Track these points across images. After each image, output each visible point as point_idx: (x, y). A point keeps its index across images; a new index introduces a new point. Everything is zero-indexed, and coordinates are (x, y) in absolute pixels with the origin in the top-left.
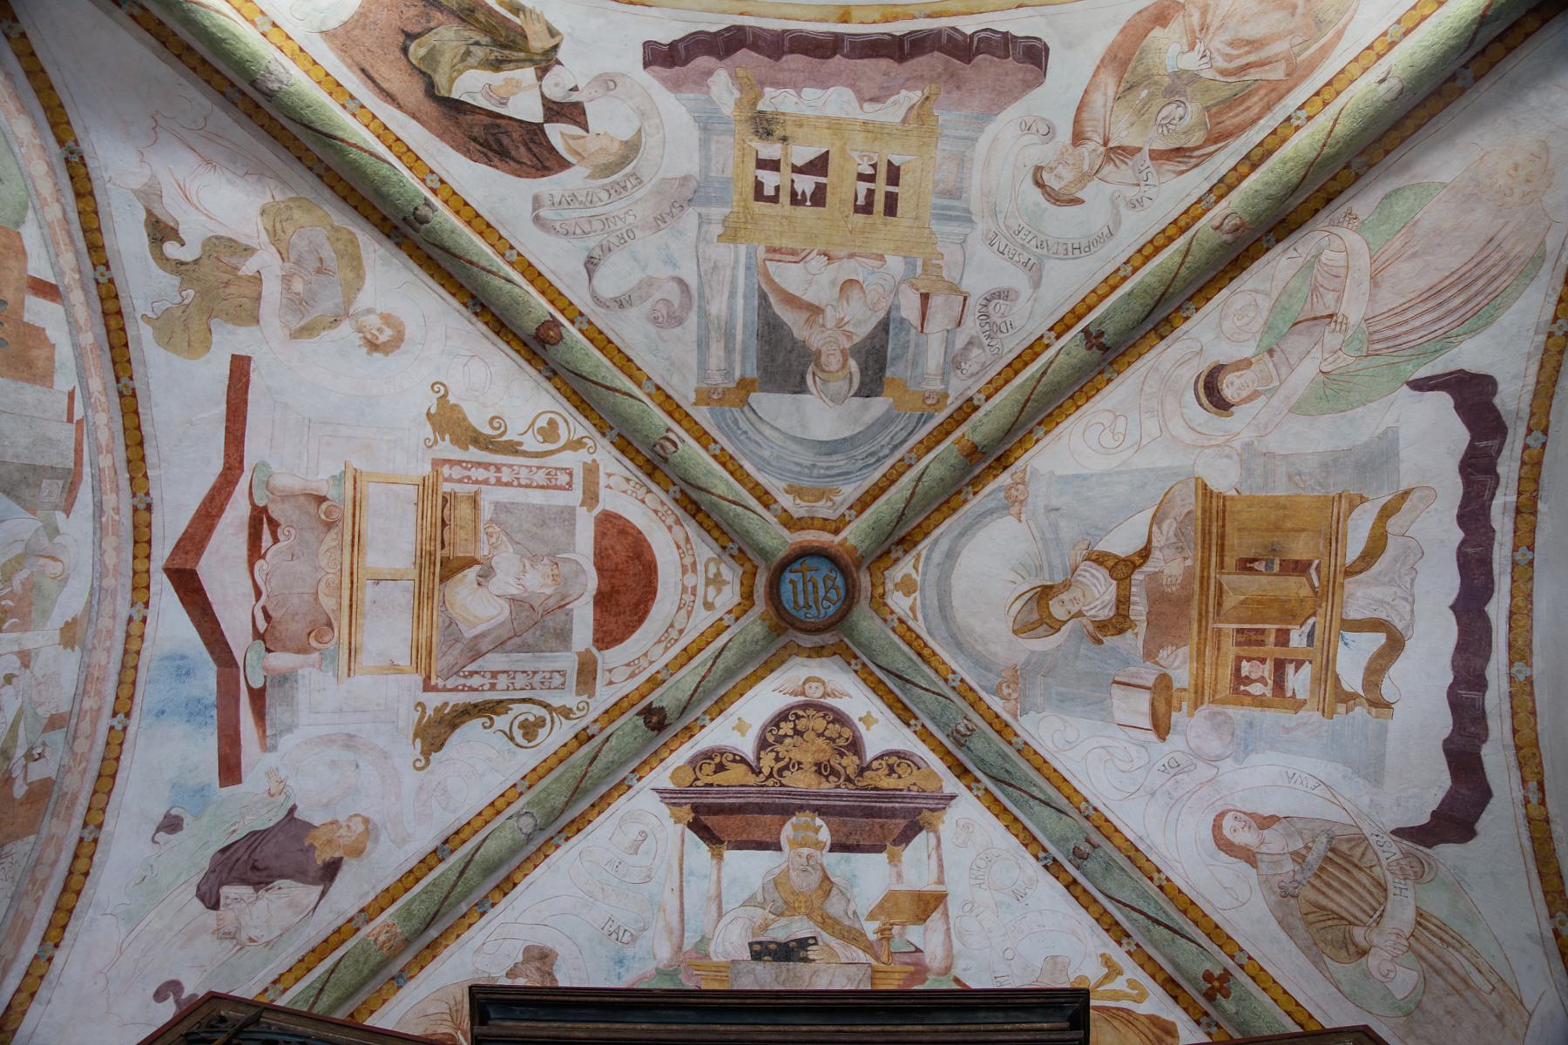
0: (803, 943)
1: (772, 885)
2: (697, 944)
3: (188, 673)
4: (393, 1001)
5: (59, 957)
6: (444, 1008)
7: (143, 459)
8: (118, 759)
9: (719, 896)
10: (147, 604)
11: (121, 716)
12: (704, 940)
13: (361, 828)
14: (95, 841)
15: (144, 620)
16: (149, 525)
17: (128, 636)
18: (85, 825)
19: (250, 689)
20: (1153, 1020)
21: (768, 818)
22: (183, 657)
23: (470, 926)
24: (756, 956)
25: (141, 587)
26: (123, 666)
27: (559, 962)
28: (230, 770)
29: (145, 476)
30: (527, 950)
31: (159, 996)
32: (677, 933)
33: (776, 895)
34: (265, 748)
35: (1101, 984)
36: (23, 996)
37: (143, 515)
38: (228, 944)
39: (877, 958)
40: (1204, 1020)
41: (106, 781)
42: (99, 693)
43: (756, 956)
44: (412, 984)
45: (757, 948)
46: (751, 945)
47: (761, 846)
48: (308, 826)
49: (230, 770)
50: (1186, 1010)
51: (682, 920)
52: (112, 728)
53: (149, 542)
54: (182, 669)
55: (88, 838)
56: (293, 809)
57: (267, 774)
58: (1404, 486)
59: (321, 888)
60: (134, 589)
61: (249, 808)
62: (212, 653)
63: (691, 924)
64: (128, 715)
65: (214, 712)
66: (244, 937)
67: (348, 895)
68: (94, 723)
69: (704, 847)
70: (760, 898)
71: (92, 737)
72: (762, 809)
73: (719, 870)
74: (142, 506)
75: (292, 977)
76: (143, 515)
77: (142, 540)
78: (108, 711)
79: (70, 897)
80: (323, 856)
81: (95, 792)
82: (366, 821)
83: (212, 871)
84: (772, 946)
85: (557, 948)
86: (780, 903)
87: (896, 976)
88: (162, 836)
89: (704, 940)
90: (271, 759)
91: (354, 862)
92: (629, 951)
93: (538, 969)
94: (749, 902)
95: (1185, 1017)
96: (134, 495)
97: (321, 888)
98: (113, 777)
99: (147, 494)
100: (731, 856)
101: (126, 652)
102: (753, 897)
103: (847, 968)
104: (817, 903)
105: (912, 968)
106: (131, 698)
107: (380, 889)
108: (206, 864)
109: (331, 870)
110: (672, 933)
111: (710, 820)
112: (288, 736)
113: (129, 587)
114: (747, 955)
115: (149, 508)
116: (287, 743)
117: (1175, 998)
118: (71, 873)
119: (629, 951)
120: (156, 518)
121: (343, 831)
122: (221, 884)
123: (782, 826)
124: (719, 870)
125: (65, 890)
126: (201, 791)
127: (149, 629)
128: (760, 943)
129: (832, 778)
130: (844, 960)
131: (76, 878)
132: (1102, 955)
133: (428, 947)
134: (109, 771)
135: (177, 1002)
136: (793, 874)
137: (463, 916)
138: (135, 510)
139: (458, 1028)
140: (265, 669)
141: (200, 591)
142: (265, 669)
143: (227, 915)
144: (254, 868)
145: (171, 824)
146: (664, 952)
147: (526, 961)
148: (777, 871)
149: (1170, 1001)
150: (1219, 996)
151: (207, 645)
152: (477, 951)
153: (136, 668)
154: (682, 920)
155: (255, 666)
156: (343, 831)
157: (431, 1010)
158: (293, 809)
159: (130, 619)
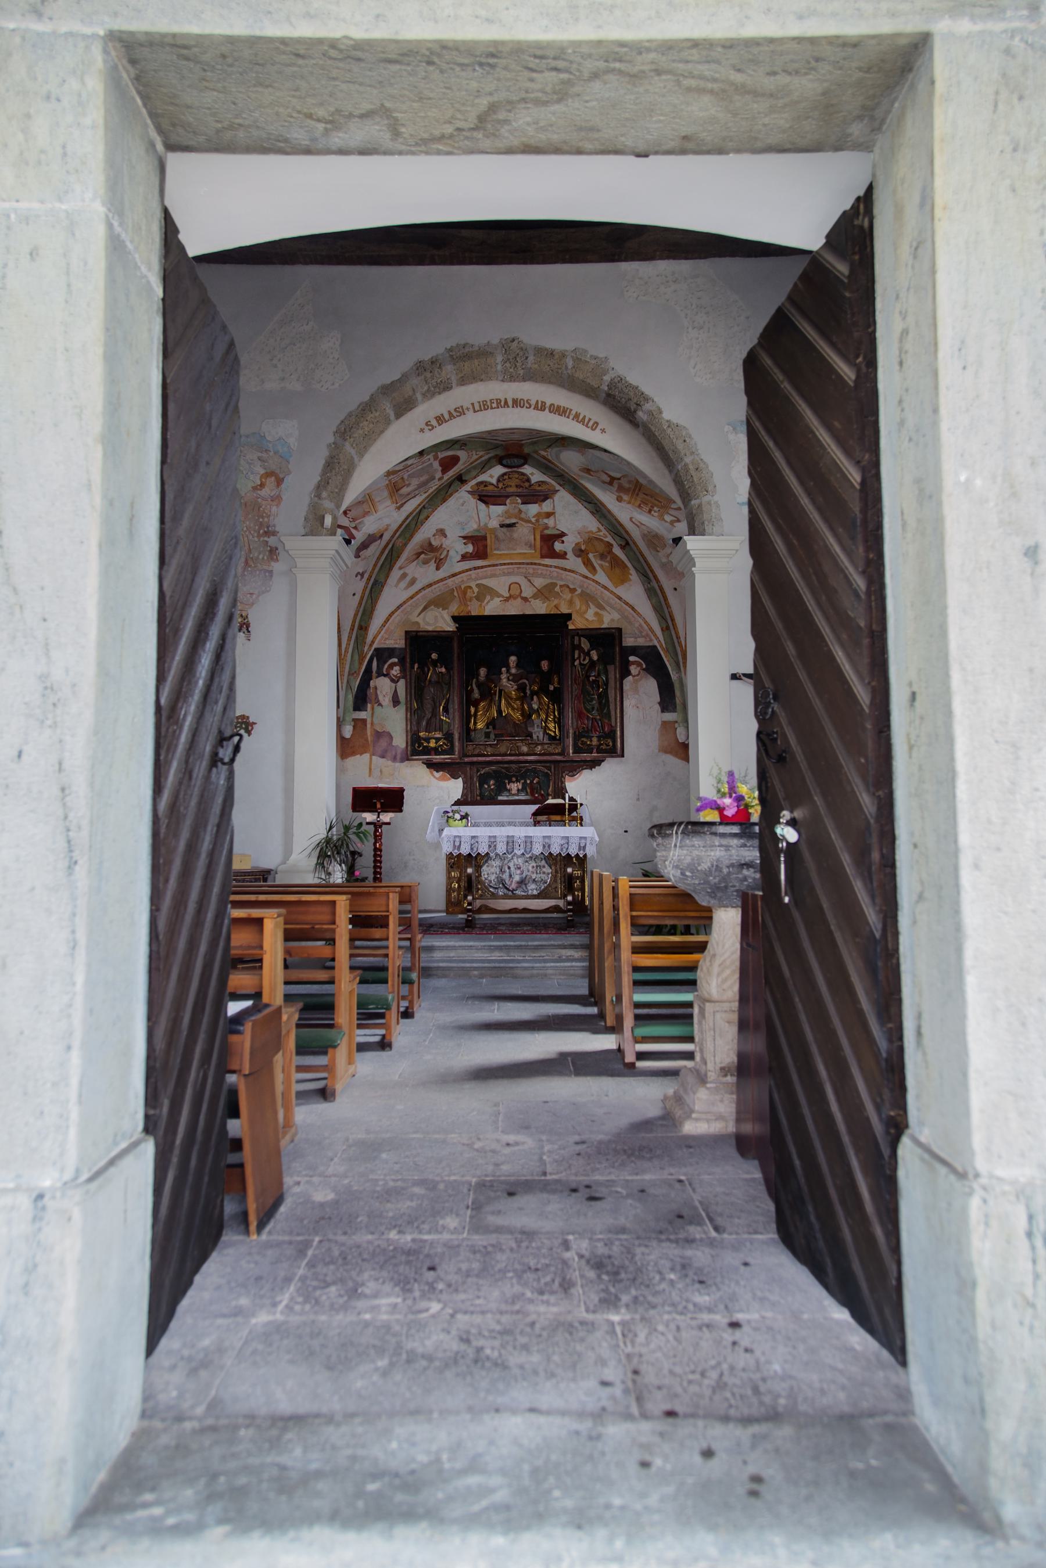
109: (381, 536)
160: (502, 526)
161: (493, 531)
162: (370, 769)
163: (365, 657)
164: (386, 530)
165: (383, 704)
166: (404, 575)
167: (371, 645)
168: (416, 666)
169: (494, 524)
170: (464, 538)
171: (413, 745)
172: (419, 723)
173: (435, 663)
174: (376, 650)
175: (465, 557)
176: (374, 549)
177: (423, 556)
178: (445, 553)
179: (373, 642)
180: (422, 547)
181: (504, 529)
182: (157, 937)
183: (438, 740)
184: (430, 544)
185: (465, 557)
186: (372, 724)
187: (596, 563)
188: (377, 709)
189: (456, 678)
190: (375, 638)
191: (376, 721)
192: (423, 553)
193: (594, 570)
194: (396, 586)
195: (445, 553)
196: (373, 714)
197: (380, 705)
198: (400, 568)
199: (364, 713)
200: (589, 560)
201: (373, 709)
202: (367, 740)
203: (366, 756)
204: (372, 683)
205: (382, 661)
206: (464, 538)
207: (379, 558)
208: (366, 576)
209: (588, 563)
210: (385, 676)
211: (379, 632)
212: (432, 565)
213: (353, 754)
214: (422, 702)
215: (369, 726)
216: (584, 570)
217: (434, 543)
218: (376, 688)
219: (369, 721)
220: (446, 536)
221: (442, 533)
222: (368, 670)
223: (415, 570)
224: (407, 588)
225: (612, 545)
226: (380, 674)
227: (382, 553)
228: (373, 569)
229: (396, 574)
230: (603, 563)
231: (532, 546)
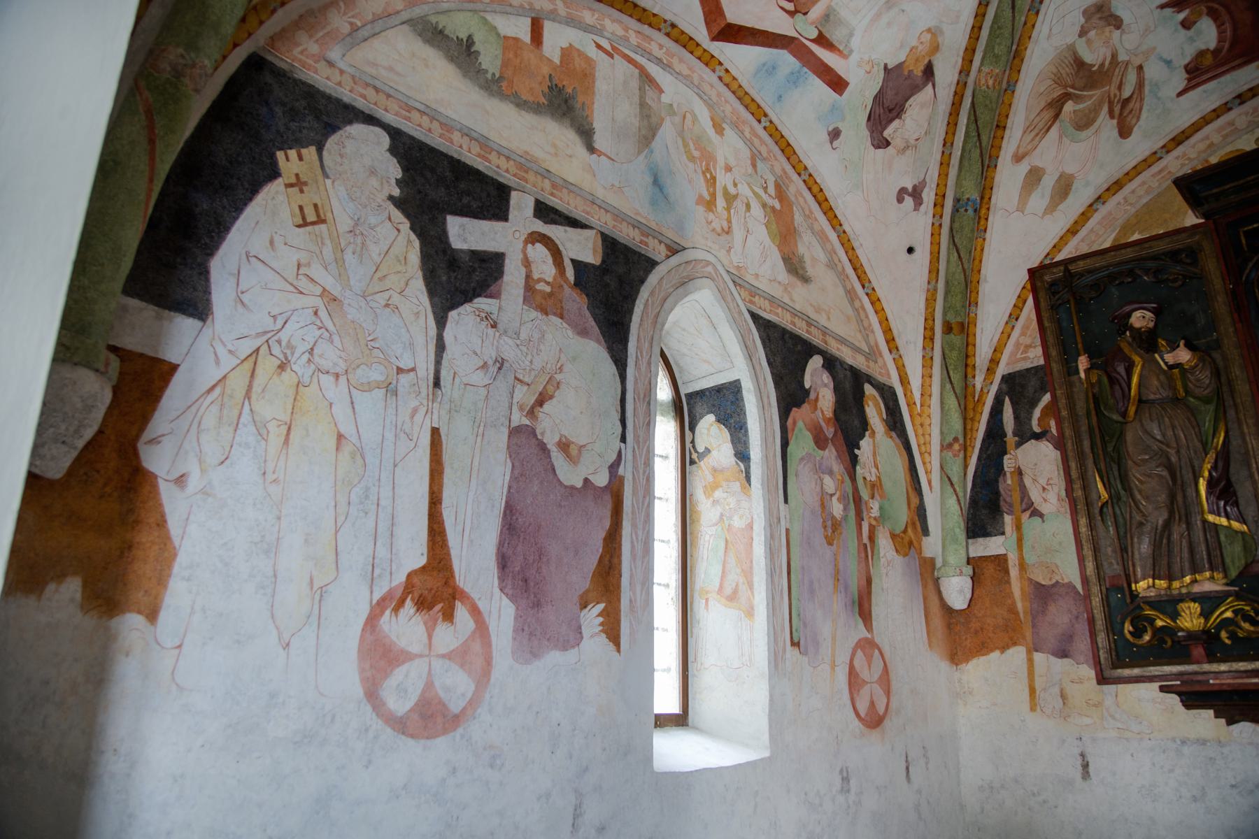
3: (774, 68)
4: (1015, 101)
5: (846, 227)
6: (1049, 82)
7: (644, 10)
8: (782, 136)
10: (720, 64)
11: (763, 119)
13: (929, 36)
14: (810, 175)
15: (727, 71)
16: (683, 33)
17: (727, 85)
18: (799, 174)
19: (812, 41)
22: (764, 65)
23: (1033, 26)
25: (709, 60)
26: (739, 99)
28: (837, 84)
29: (655, 15)
30: (1084, 13)
31: (900, 200)
34: (845, 57)
36: (850, 252)
37: (675, 32)
38: (908, 152)
41: (788, 150)
42: (743, 122)
44: (1020, 84)
48: (900, 66)
49: (837, 84)
52: (765, 128)
53: (691, 39)
54: (770, 69)
55: (806, 178)
56: (886, 65)
57: (859, 66)
58: (1054, 131)
59: (930, 85)
60: (707, 65)
61: (864, 89)
62: (776, 47)
64: (766, 115)
65: (805, 69)
66: (912, 142)
67: (946, 74)
68: (756, 136)
71: (763, 142)
74: (669, 29)
75: (950, 135)
76: (675, 32)
77: (686, 42)
78: (755, 123)
79: (825, 205)
80: (918, 71)
81: (788, 159)
82: (929, 30)
83: (872, 132)
88: (836, 143)
90: (854, 58)
91: (938, 55)
93: (1100, 18)
96: (660, 30)
97: (930, 85)
98: (789, 145)
99: (665, 21)
101: (734, 93)
106: (759, 107)
107: (961, 53)
108: (866, 133)
109: (929, 72)
112: (853, 39)
113: (703, 66)
115: (673, 26)
116: (855, 43)
118: (815, 196)
120: (683, 26)
121: (920, 48)
122: (882, 133)
125: (820, 204)
126: (834, 108)
127: (733, 72)
131: (819, 196)
134: (784, 145)
135: (910, 195)
137: (1025, 23)
138: (668, 35)
139: (1066, 87)
140: (812, 23)
141: (740, 29)
142: (812, 23)
143: (897, 142)
144: (890, 111)
145: (835, 134)
151: (770, 46)
152: (1049, 37)
153: (746, 93)
155: (805, 29)
156: (920, 48)
157: (1042, 89)
158: (886, 65)
159: (720, 78)
162: (1032, 691)
163: (981, 402)
164: (936, 48)
165: (1045, 508)
166: (1035, 176)
167: (990, 371)
168: (1083, 363)
171: (1113, 627)
172: (1124, 550)
173: (1148, 342)
174: (1007, 379)
175: (1198, 72)
176: (923, 116)
177: (1069, 107)
179: (994, 362)
180: (1058, 80)
183: (1209, 602)
184: (1080, 64)
185: (1198, 72)
186: (1023, 566)
188: (1031, 526)
189: (1237, 371)
190: (998, 350)
191: (1030, 558)
192: (1066, 97)
194: (1021, 208)
195: (1132, 78)
196: (1020, 540)
197: (1036, 513)
198: (1018, 158)
199: (1000, 539)
201: (1018, 527)
202: (1013, 610)
203: (1017, 654)
204: (1008, 463)
205: (1023, 406)
207: (947, 143)
208: (929, 196)
210: (1037, 437)
211: (1006, 335)
212: (1106, 126)
213: (983, 648)
214: (1124, 478)
215: (1014, 572)
217: (1088, 57)
218: (1020, 473)
219: (1013, 559)
220: (1117, 23)
222: (995, 433)
223: (1060, 152)
224: (1052, 208)
226: (1025, 435)
227: (952, 124)
228: (943, 175)
229: (1008, 177)
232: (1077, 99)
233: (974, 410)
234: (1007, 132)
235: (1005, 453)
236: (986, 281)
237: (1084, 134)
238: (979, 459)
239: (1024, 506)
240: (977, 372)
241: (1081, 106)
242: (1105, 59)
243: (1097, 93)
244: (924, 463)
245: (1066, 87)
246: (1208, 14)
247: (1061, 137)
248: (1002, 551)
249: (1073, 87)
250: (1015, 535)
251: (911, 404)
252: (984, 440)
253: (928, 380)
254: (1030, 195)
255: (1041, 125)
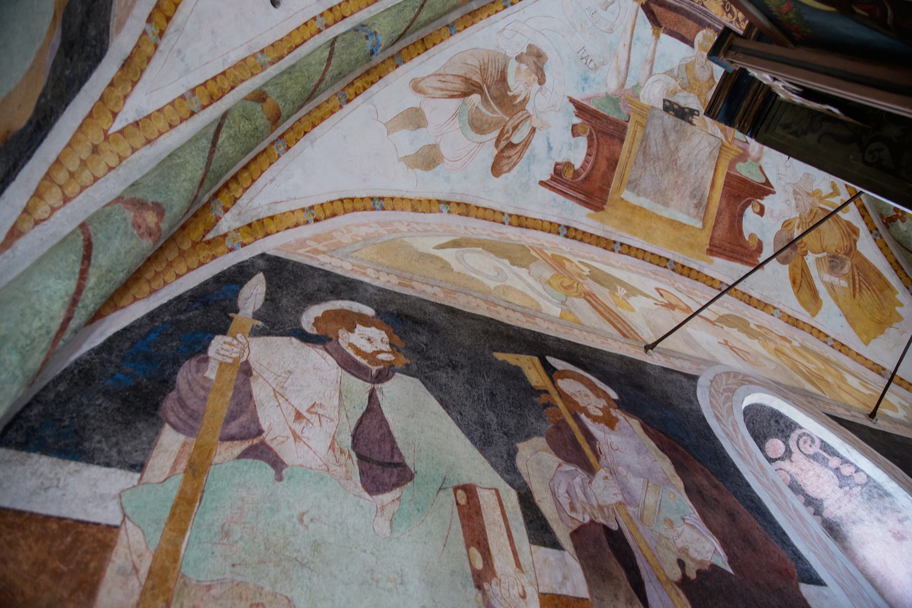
0: (692, 112)
1: (684, 68)
2: (634, 87)
4: (446, 43)
6: (477, 64)
9: (652, 61)
12: (638, 86)
20: (849, 224)
21: (690, 23)
24: (666, 109)
27: (548, 63)
32: (623, 75)
33: (685, 75)
35: (827, 197)
39: (726, 138)
40: (875, 232)
43: (666, 109)
45: (667, 104)
46: (664, 100)
47: (683, 39)
50: (867, 224)
51: (627, 68)
58: (456, 102)
63: (632, 73)
69: (649, 25)
70: (675, 73)
72: (689, 15)
73: (656, 44)
84: (676, 107)
85: (548, 54)
86: (686, 81)
87: (733, 152)
89: (638, 86)
92: (592, 75)
93: (535, 63)
94: (669, 73)
95: (865, 227)
100: (664, 37)
102: (671, 71)
103: (711, 137)
104: (704, 92)
105: (742, 151)
110: (619, 73)
111: (656, 9)
114: (661, 106)
117: (863, 217)
119: (592, 75)
123: (698, 31)
124: (656, 44)
128: (670, 102)
129: (729, 15)
130: (710, 132)
132: (832, 182)
133: (470, 14)
136: (697, 67)
146: (613, 85)
147: (528, 54)
148: (689, 60)
149: (860, 217)
150: (899, 220)
154: (627, 68)
160: (670, 107)
161: (646, 112)
169: (653, 94)
170: (581, 109)
177: (476, 98)
178: (524, 132)
181: (669, 120)
182: (806, 394)
187: (820, 278)
188: (234, 479)
193: (812, 300)
196: (186, 505)
197: (261, 452)
199: (117, 480)
200: (805, 271)
201: (197, 468)
206: (581, 109)
209: (802, 282)
216: (790, 302)
219: (135, 548)
220: (541, 82)
221: (536, 59)
225: (855, 231)
229: (393, 92)
230: (835, 280)
231: (702, 205)
232: (485, 100)
233: (195, 244)
234: (424, 56)
235: (224, 332)
236: (312, 142)
237: (471, 134)
238: (152, 316)
239: (234, 428)
240: (234, 210)
241: (484, 110)
242: (519, 95)
243: (499, 114)
244: (38, 195)
245: (484, 81)
246: (588, 137)
247: (455, 114)
248: (108, 515)
249: (488, 88)
250: (174, 485)
251: (107, 105)
252: (179, 298)
253: (162, 124)
254: (404, 127)
255: (449, 86)
